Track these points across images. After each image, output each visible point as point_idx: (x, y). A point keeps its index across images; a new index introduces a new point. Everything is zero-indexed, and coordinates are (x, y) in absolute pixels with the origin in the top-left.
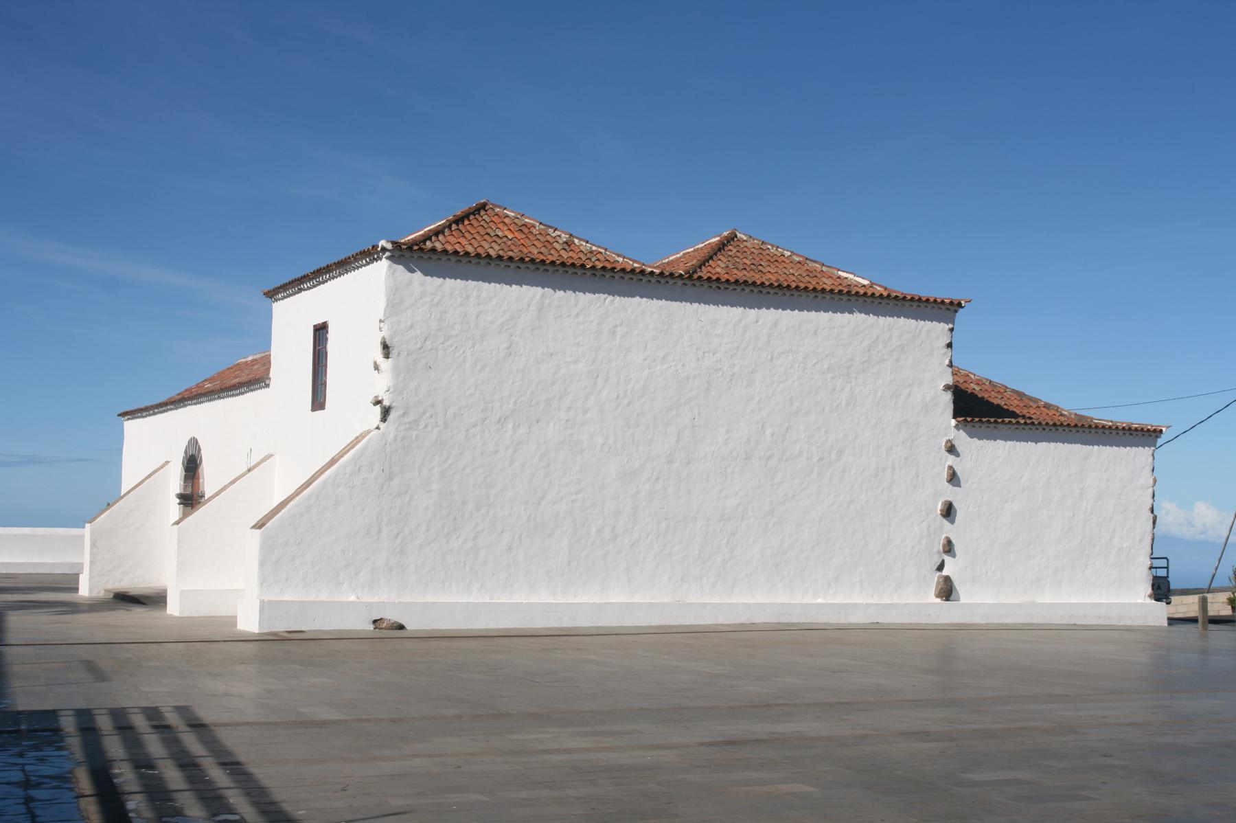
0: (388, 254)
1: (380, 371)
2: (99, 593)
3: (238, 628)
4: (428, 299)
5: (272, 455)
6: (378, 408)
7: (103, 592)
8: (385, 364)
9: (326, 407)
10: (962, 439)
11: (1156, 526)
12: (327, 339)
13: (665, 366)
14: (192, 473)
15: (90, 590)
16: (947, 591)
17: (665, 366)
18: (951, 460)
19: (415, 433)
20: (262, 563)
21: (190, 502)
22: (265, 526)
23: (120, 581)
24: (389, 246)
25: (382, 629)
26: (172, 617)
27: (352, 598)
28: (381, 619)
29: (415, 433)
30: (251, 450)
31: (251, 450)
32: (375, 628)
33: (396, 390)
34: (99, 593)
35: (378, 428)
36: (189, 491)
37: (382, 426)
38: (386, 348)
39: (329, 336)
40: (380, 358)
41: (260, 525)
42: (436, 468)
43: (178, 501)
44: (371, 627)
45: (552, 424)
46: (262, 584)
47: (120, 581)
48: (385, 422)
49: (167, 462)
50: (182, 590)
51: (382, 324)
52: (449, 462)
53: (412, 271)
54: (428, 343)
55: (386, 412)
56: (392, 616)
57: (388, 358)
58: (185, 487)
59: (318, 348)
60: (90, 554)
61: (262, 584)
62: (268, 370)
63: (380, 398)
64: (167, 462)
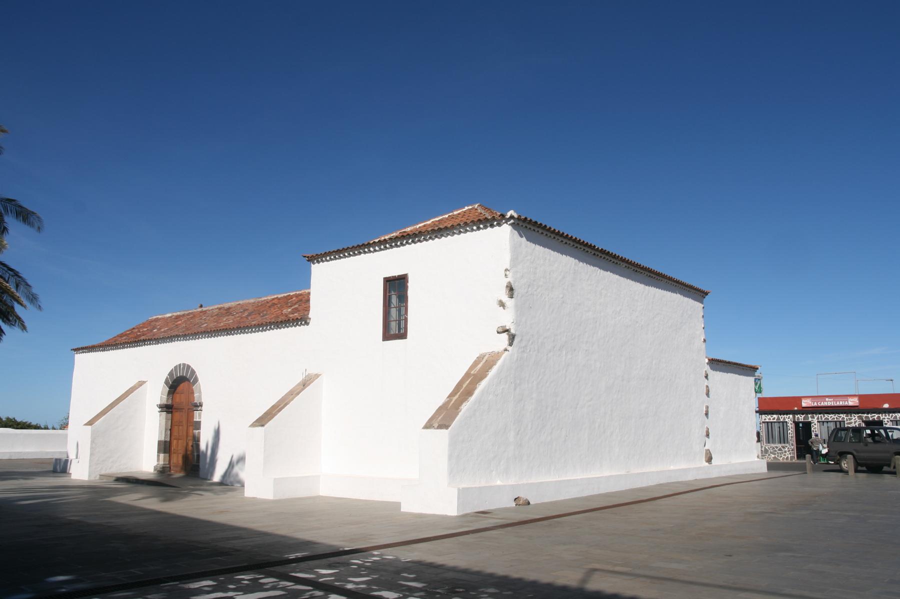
0: (512, 221)
1: (506, 308)
2: (95, 478)
3: (402, 510)
4: (529, 258)
5: (144, 382)
6: (505, 336)
7: (98, 477)
8: (509, 302)
9: (408, 337)
10: (712, 373)
11: (34, 423)
12: (407, 287)
13: (620, 318)
14: (173, 390)
15: (89, 476)
16: (709, 459)
17: (620, 318)
18: (706, 383)
19: (525, 355)
20: (450, 457)
21: (170, 410)
22: (451, 427)
23: (110, 468)
24: (516, 216)
25: (519, 505)
26: (254, 501)
27: (499, 483)
28: (518, 497)
29: (525, 355)
30: (306, 370)
31: (306, 370)
32: (516, 505)
33: (517, 323)
34: (96, 477)
35: (506, 350)
36: (170, 402)
37: (510, 348)
38: (511, 290)
39: (409, 284)
40: (505, 298)
41: (90, 423)
42: (535, 382)
43: (159, 410)
44: (514, 504)
45: (580, 353)
46: (450, 475)
47: (110, 468)
48: (511, 346)
49: (141, 384)
50: (275, 479)
51: (508, 273)
52: (540, 377)
53: (521, 237)
54: (530, 289)
55: (512, 338)
56: (524, 495)
57: (512, 298)
58: (168, 399)
59: (388, 294)
60: (91, 448)
61: (450, 475)
62: (307, 309)
63: (508, 328)
64: (141, 384)
